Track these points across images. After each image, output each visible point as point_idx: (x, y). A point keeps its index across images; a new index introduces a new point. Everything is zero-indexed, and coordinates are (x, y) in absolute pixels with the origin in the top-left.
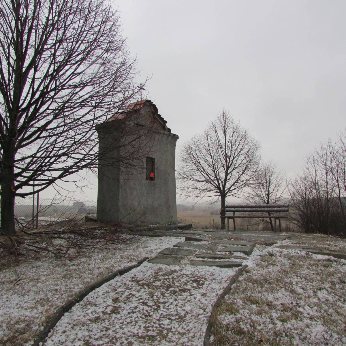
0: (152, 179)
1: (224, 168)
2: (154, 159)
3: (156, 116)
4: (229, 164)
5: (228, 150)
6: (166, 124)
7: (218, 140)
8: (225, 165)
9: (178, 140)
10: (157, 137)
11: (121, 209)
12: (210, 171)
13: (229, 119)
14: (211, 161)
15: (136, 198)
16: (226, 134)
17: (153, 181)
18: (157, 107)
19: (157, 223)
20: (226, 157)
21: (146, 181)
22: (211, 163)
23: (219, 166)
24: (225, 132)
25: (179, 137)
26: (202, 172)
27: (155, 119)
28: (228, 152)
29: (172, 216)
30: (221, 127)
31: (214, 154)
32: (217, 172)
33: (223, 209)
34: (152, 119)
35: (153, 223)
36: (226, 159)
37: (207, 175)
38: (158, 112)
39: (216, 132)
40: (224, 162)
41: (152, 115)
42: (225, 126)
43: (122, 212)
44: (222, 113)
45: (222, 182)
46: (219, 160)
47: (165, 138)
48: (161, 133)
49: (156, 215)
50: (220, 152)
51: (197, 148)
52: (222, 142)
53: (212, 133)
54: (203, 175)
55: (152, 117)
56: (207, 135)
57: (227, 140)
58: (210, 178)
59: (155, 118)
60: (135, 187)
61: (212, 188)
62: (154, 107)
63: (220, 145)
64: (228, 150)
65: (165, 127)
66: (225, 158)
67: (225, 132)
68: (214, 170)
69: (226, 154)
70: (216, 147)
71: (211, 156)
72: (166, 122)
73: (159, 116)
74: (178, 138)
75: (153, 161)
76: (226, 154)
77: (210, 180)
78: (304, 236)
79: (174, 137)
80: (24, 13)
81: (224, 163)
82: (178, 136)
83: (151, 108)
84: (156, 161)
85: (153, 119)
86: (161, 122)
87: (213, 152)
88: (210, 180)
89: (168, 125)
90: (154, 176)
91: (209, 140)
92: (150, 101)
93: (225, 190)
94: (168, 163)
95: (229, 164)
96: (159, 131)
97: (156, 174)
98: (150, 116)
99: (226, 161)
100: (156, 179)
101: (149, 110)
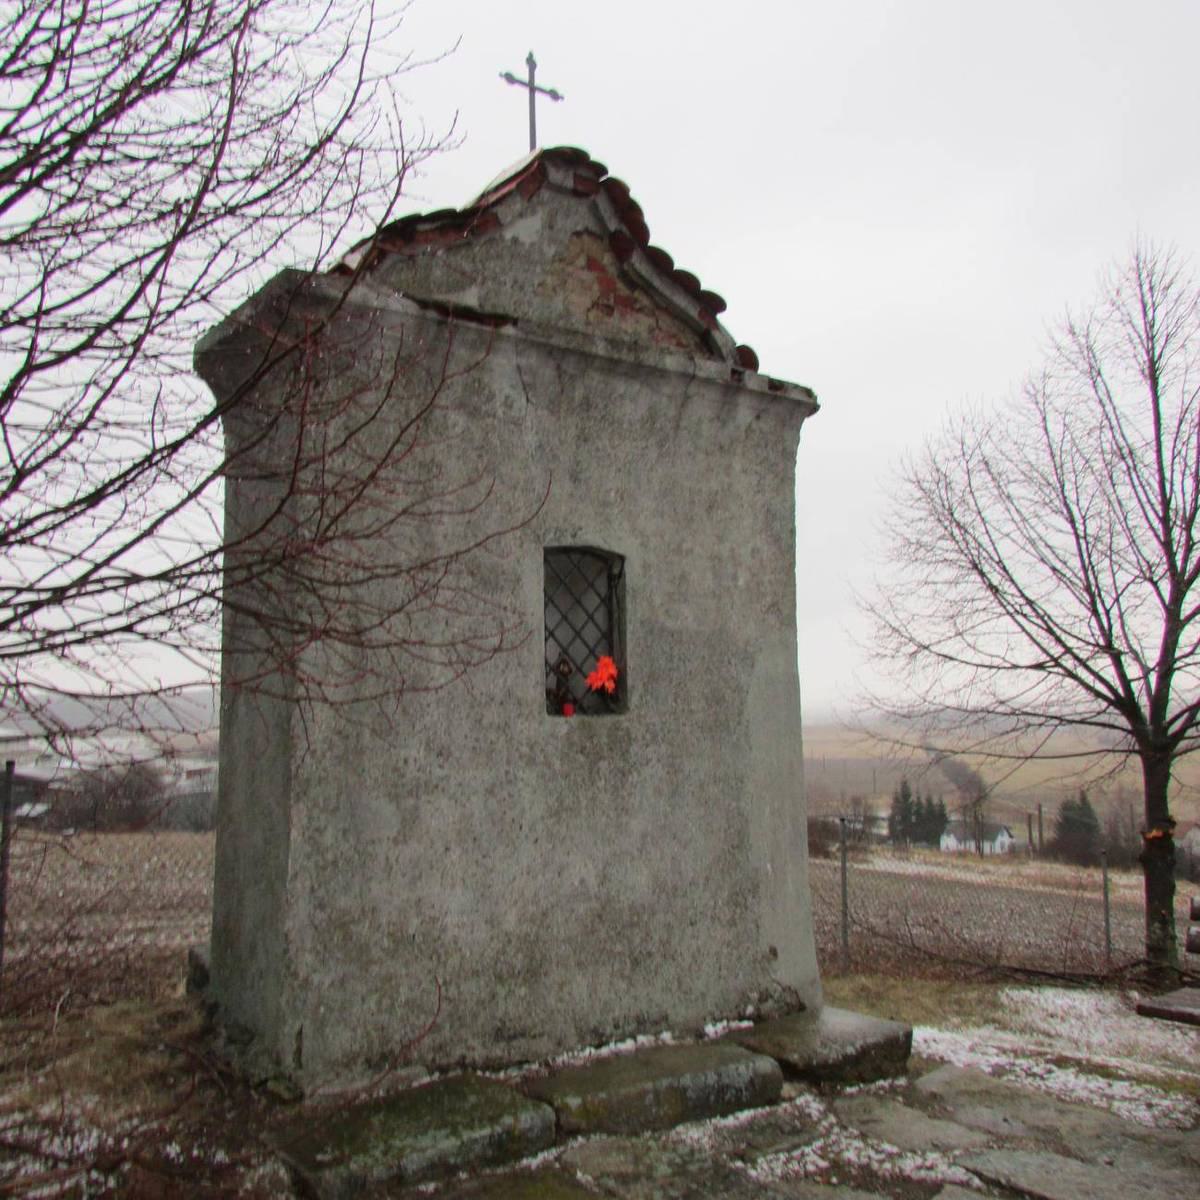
0: (611, 700)
1: (1155, 584)
2: (622, 558)
3: (637, 262)
4: (1185, 560)
5: (1177, 477)
6: (721, 317)
7: (1110, 420)
8: (1161, 570)
9: (809, 425)
10: (633, 402)
11: (309, 958)
12: (1066, 607)
13: (1173, 292)
14: (1075, 550)
15: (455, 855)
16: (1162, 381)
17: (608, 720)
18: (634, 194)
19: (642, 1024)
20: (1165, 520)
21: (548, 719)
22: (1075, 563)
23: (1123, 578)
24: (1153, 375)
25: (819, 401)
26: (1020, 618)
27: (632, 285)
28: (1177, 488)
29: (774, 952)
30: (1128, 347)
31: (1084, 503)
32: (1114, 612)
33: (1154, 833)
34: (607, 286)
35: (609, 1030)
36: (1168, 530)
37: (1050, 631)
38: (642, 232)
39: (1094, 373)
40: (1153, 551)
41: (607, 259)
42: (1151, 338)
43: (316, 978)
44: (1127, 261)
45: (1146, 671)
46: (1121, 542)
47: (703, 406)
48: (662, 373)
49: (636, 963)
50: (1124, 491)
51: (980, 479)
52: (1139, 432)
53: (1070, 386)
54: (1024, 629)
55: (612, 271)
56: (1039, 399)
57: (1169, 422)
58: (1068, 650)
59: (633, 282)
60: (447, 778)
61: (1084, 703)
62: (617, 192)
63: (1125, 454)
64: (1177, 477)
65: (716, 335)
66: (1157, 524)
67: (1153, 375)
68: (1093, 602)
69: (1166, 503)
70: (1098, 465)
71: (1072, 522)
72: (715, 303)
73: (660, 260)
74: (814, 408)
75: (616, 571)
76: (1166, 503)
77: (1068, 662)
78: (995, 513)
79: (775, 398)
80: (234, 14)
81: (1154, 560)
82: (808, 392)
83: (594, 209)
84: (633, 574)
85: (622, 289)
86: (681, 301)
87: (1086, 493)
88: (1068, 662)
89: (736, 324)
90: (620, 680)
91: (1055, 429)
92: (572, 159)
93: (1169, 716)
94: (741, 582)
95: (1185, 560)
96: (650, 358)
97: (631, 663)
98: (592, 264)
99: (1167, 545)
100: (634, 700)
101: (579, 216)
